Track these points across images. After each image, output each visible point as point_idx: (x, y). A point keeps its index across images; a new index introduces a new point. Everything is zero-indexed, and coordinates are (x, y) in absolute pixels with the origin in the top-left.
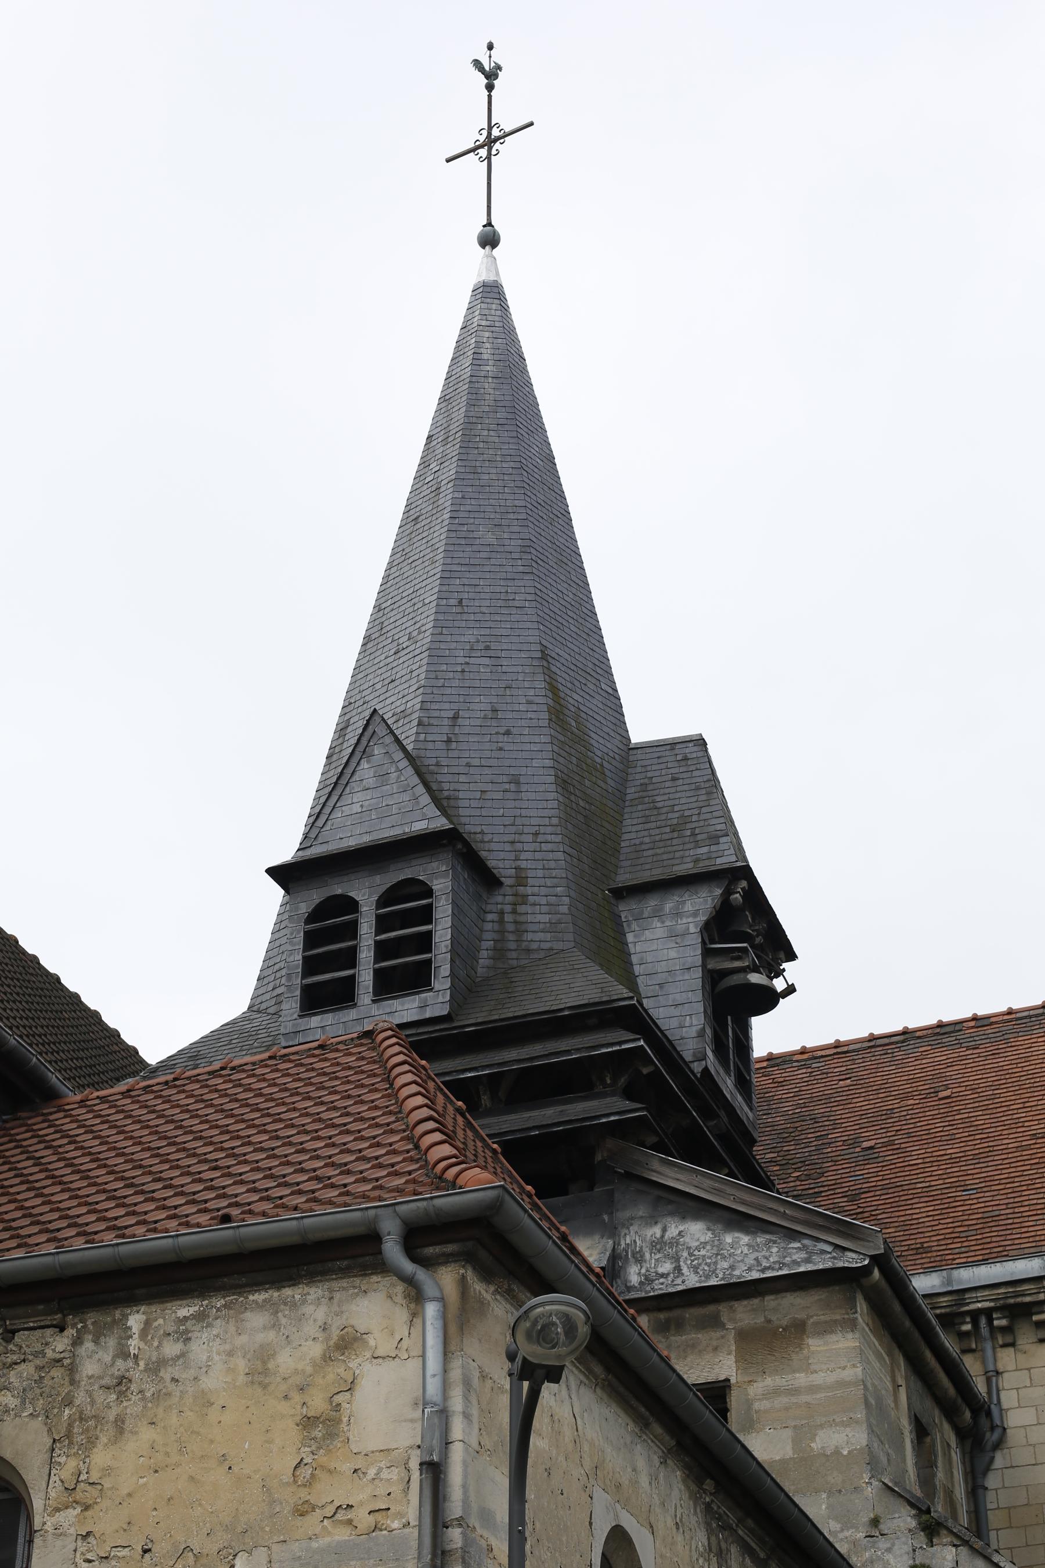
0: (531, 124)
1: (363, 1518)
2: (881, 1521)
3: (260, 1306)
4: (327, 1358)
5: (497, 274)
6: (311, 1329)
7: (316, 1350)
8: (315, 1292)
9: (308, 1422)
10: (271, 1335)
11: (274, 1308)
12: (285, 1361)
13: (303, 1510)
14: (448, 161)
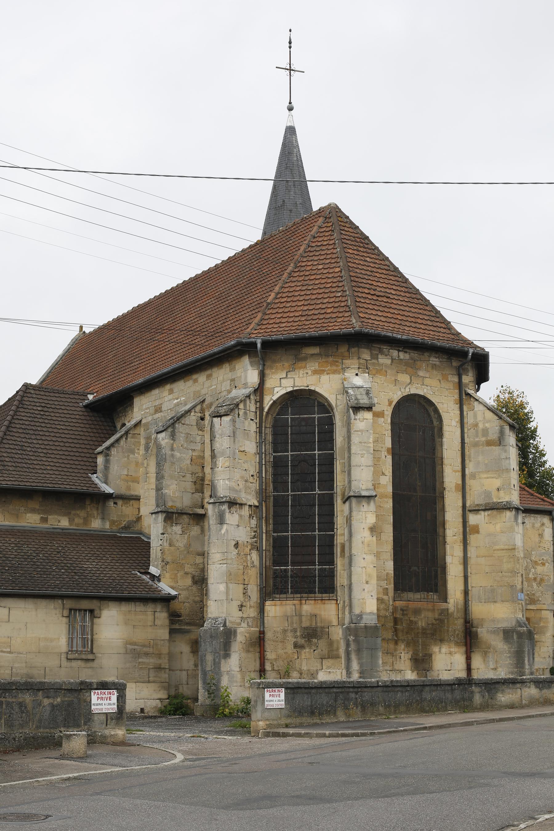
0: (304, 72)
1: (546, 549)
2: (191, 655)
3: (533, 516)
4: (541, 526)
5: (294, 124)
6: (539, 521)
7: (540, 525)
8: (539, 516)
9: (539, 535)
10: (534, 521)
11: (534, 517)
12: (536, 525)
13: (539, 547)
14: (276, 67)
